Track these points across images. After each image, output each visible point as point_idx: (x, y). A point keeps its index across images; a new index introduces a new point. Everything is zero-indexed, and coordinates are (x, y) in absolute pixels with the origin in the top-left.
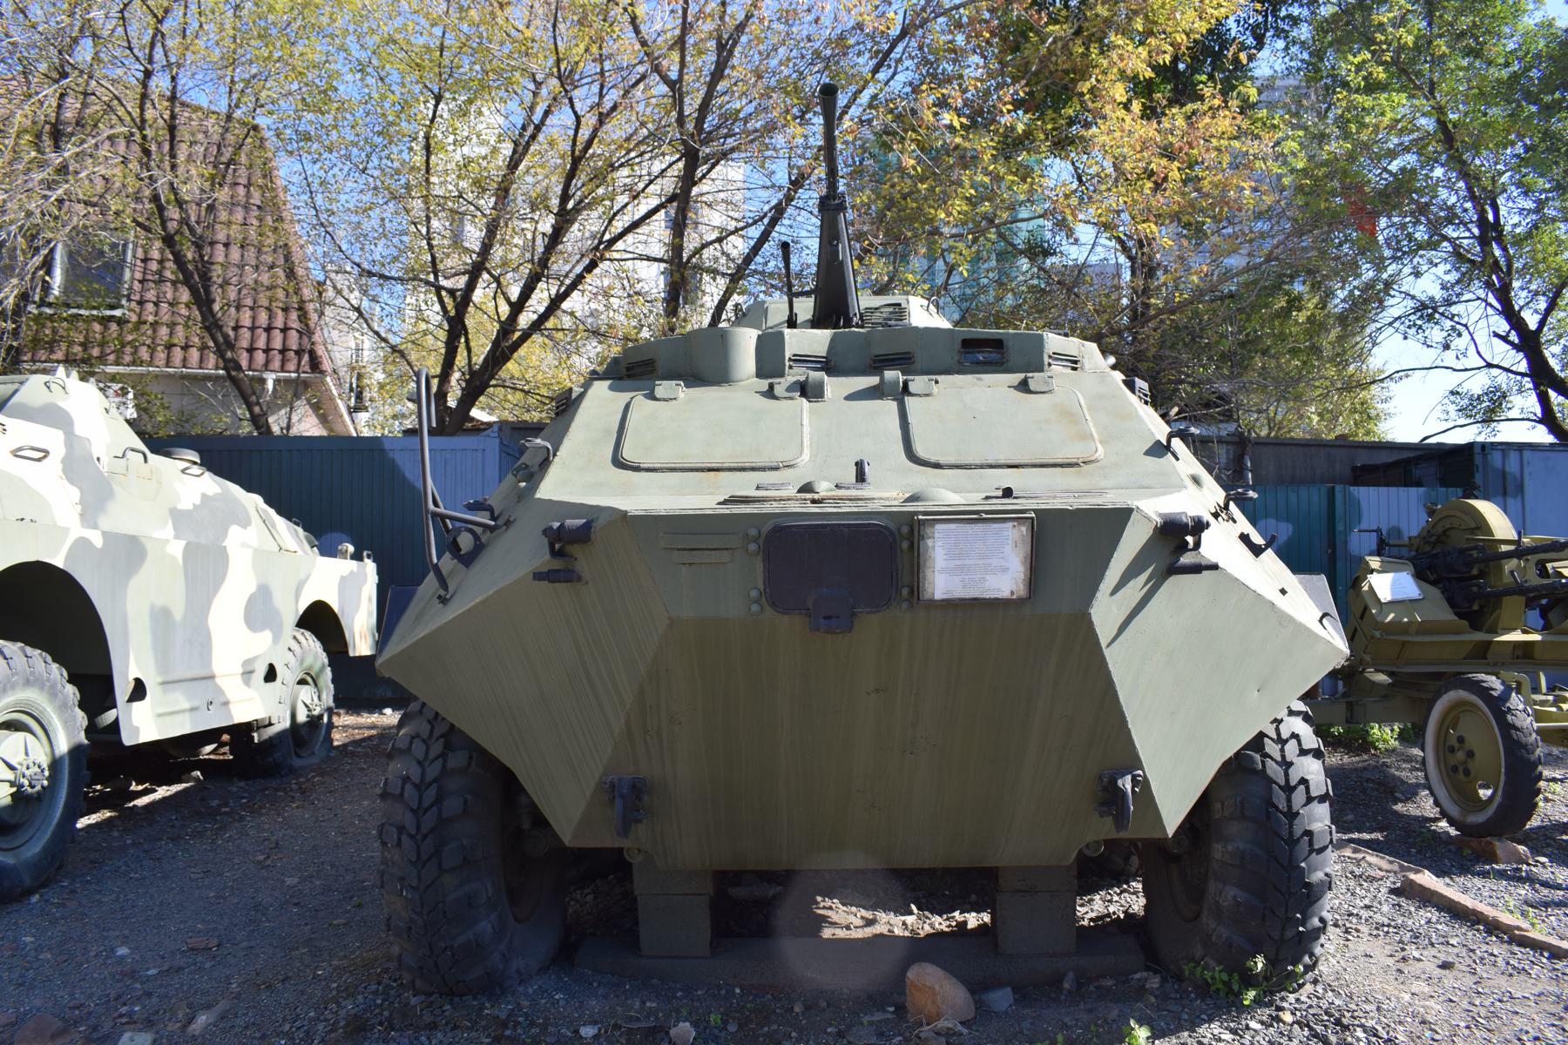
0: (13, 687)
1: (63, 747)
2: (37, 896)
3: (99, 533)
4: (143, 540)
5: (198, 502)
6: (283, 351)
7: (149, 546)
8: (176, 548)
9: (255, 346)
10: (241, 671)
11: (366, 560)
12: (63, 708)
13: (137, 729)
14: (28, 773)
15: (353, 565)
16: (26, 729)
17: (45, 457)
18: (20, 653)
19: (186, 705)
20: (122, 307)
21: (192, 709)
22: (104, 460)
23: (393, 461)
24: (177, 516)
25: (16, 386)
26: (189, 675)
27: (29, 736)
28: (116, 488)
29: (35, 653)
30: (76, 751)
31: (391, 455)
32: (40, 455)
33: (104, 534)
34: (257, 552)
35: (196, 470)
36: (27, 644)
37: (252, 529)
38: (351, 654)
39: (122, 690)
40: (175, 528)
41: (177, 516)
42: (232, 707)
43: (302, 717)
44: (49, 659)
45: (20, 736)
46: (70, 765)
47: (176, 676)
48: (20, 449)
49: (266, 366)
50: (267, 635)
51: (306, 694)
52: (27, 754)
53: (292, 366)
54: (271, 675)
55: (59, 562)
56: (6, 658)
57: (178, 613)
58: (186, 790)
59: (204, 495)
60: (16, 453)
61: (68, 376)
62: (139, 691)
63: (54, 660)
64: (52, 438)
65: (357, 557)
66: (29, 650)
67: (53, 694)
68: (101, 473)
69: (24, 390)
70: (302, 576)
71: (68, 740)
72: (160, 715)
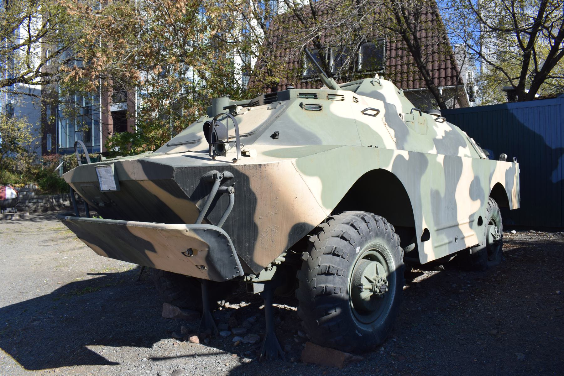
0: (370, 238)
1: (393, 267)
2: (383, 349)
3: (407, 152)
4: (426, 155)
5: (444, 135)
6: (445, 78)
7: (429, 158)
8: (440, 158)
9: (447, 67)
10: (469, 221)
11: (515, 162)
12: (393, 247)
13: (426, 255)
14: (379, 285)
15: (510, 164)
16: (380, 262)
17: (377, 114)
18: (372, 219)
19: (447, 241)
20: (383, 69)
21: (450, 243)
22: (403, 115)
23: (513, 114)
24: (437, 142)
25: (358, 85)
26: (448, 225)
27: (378, 263)
28: (409, 129)
29: (379, 218)
30: (399, 269)
31: (511, 111)
32: (374, 113)
33: (410, 153)
34: (474, 160)
35: (441, 120)
36: (376, 213)
37: (467, 148)
38: (511, 209)
39: (419, 235)
40: (437, 149)
41: (437, 142)
42: (466, 240)
43: (491, 241)
44: (386, 221)
45: (374, 263)
46: (397, 277)
47: (442, 226)
48: (366, 110)
49: (439, 85)
50: (478, 202)
51: (493, 229)
52: (377, 273)
53: (450, 83)
54: (480, 222)
55: (389, 169)
56: (366, 222)
57: (442, 194)
58: (437, 274)
59: (445, 132)
60: (364, 112)
61: (380, 78)
62: (426, 235)
63: (388, 222)
64: (378, 104)
65: (509, 160)
66: (376, 216)
67: (389, 240)
68: (402, 122)
69: (362, 85)
70: (492, 171)
71: (396, 264)
72: (436, 247)
